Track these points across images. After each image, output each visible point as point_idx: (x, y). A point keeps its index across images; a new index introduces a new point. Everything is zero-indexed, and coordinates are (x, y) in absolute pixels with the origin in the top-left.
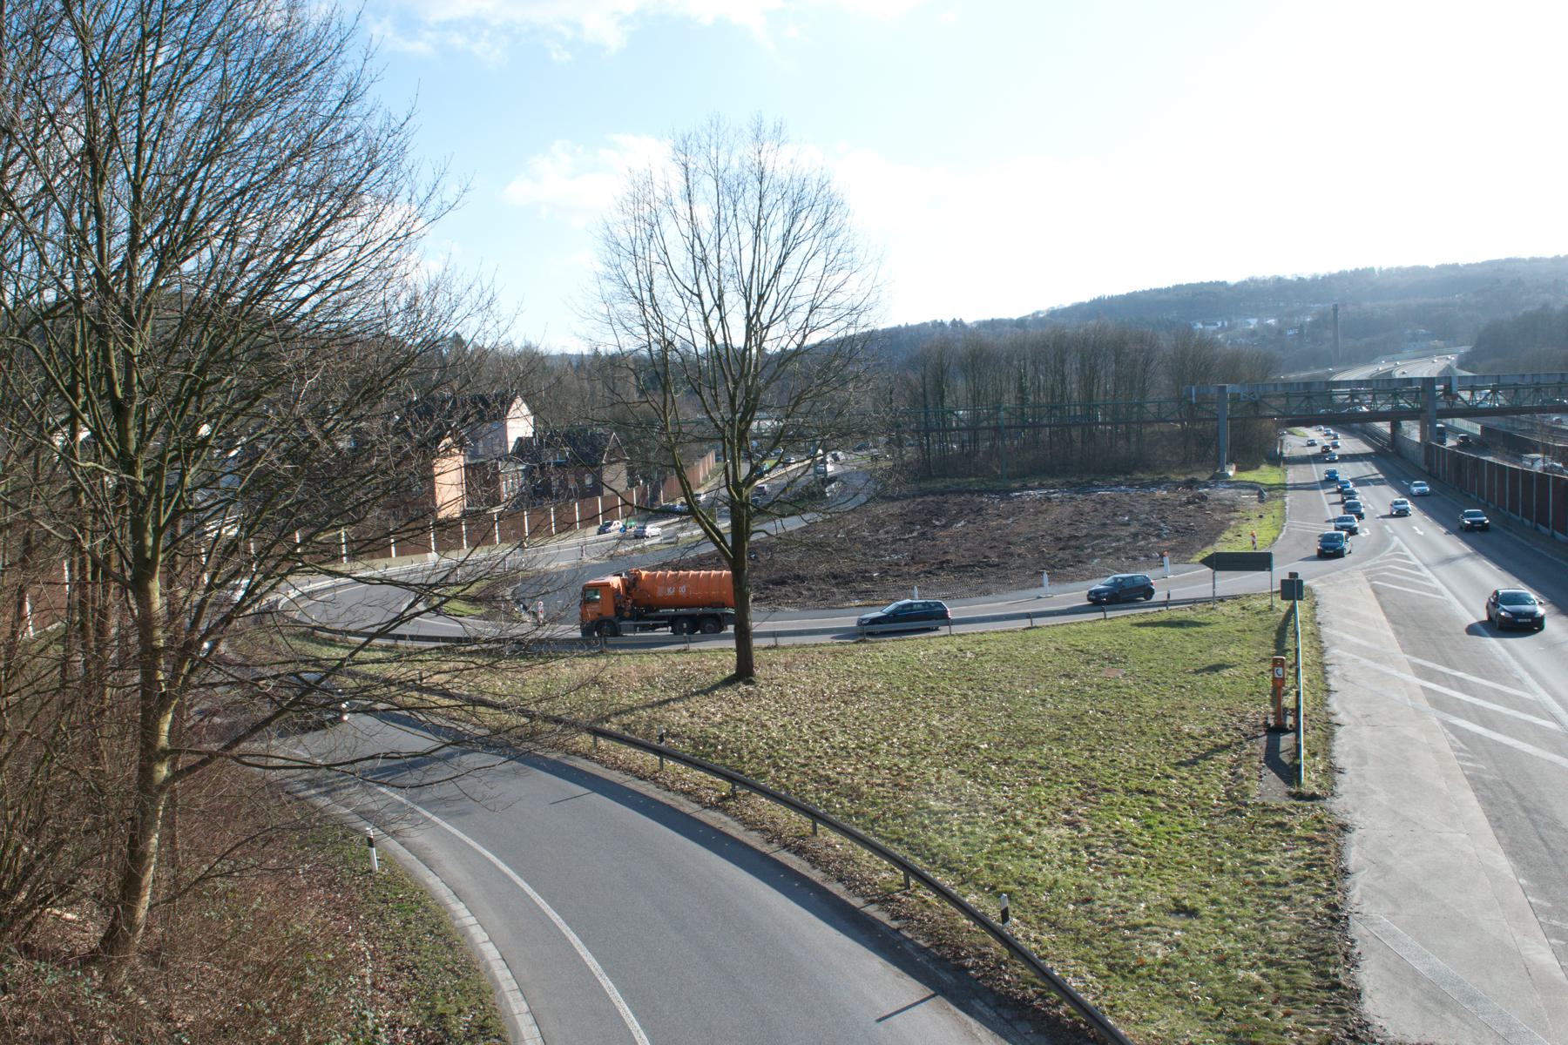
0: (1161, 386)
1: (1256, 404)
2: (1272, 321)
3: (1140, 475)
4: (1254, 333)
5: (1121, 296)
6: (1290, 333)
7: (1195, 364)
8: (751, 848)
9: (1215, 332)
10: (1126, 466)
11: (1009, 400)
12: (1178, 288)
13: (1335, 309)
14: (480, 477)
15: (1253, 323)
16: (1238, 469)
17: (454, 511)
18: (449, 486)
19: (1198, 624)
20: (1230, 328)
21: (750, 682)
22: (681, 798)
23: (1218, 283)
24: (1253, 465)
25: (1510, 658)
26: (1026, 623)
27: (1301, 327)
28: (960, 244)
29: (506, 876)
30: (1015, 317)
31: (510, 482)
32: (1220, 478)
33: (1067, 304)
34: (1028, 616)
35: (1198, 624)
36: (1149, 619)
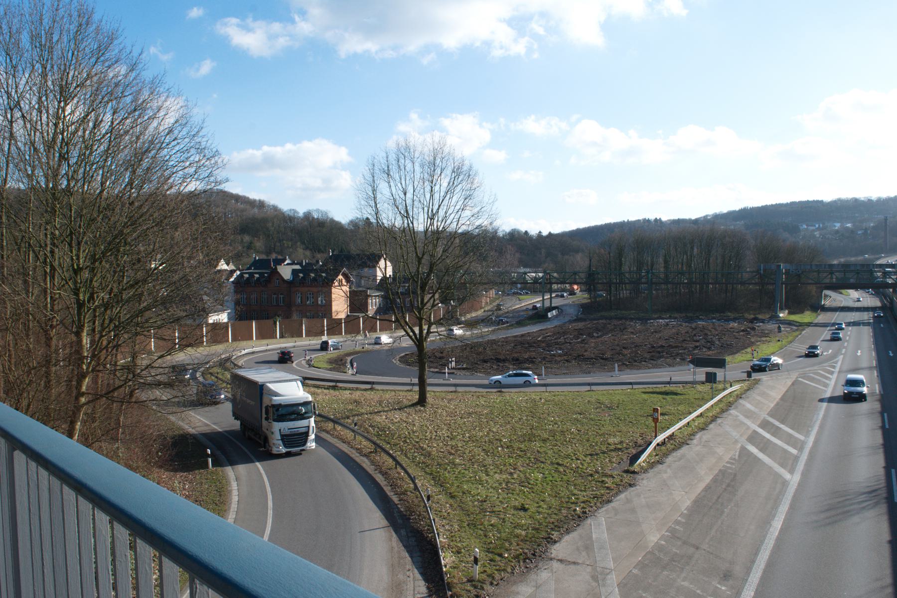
0: (749, 265)
1: (799, 276)
2: (849, 225)
3: (729, 314)
4: (837, 232)
5: (758, 208)
6: (860, 232)
7: (769, 253)
8: (367, 472)
9: (813, 231)
10: (725, 307)
11: (660, 267)
12: (793, 203)
13: (886, 219)
14: (357, 302)
15: (838, 225)
16: (790, 313)
17: (342, 316)
18: (340, 306)
19: (676, 394)
20: (822, 229)
21: (424, 406)
22: (354, 451)
23: (818, 202)
24: (801, 311)
25: (818, 422)
26: (588, 388)
27: (866, 230)
28: (556, 179)
29: (261, 474)
30: (693, 218)
31: (373, 304)
32: (774, 317)
33: (725, 211)
34: (589, 384)
35: (676, 394)
36: (658, 390)
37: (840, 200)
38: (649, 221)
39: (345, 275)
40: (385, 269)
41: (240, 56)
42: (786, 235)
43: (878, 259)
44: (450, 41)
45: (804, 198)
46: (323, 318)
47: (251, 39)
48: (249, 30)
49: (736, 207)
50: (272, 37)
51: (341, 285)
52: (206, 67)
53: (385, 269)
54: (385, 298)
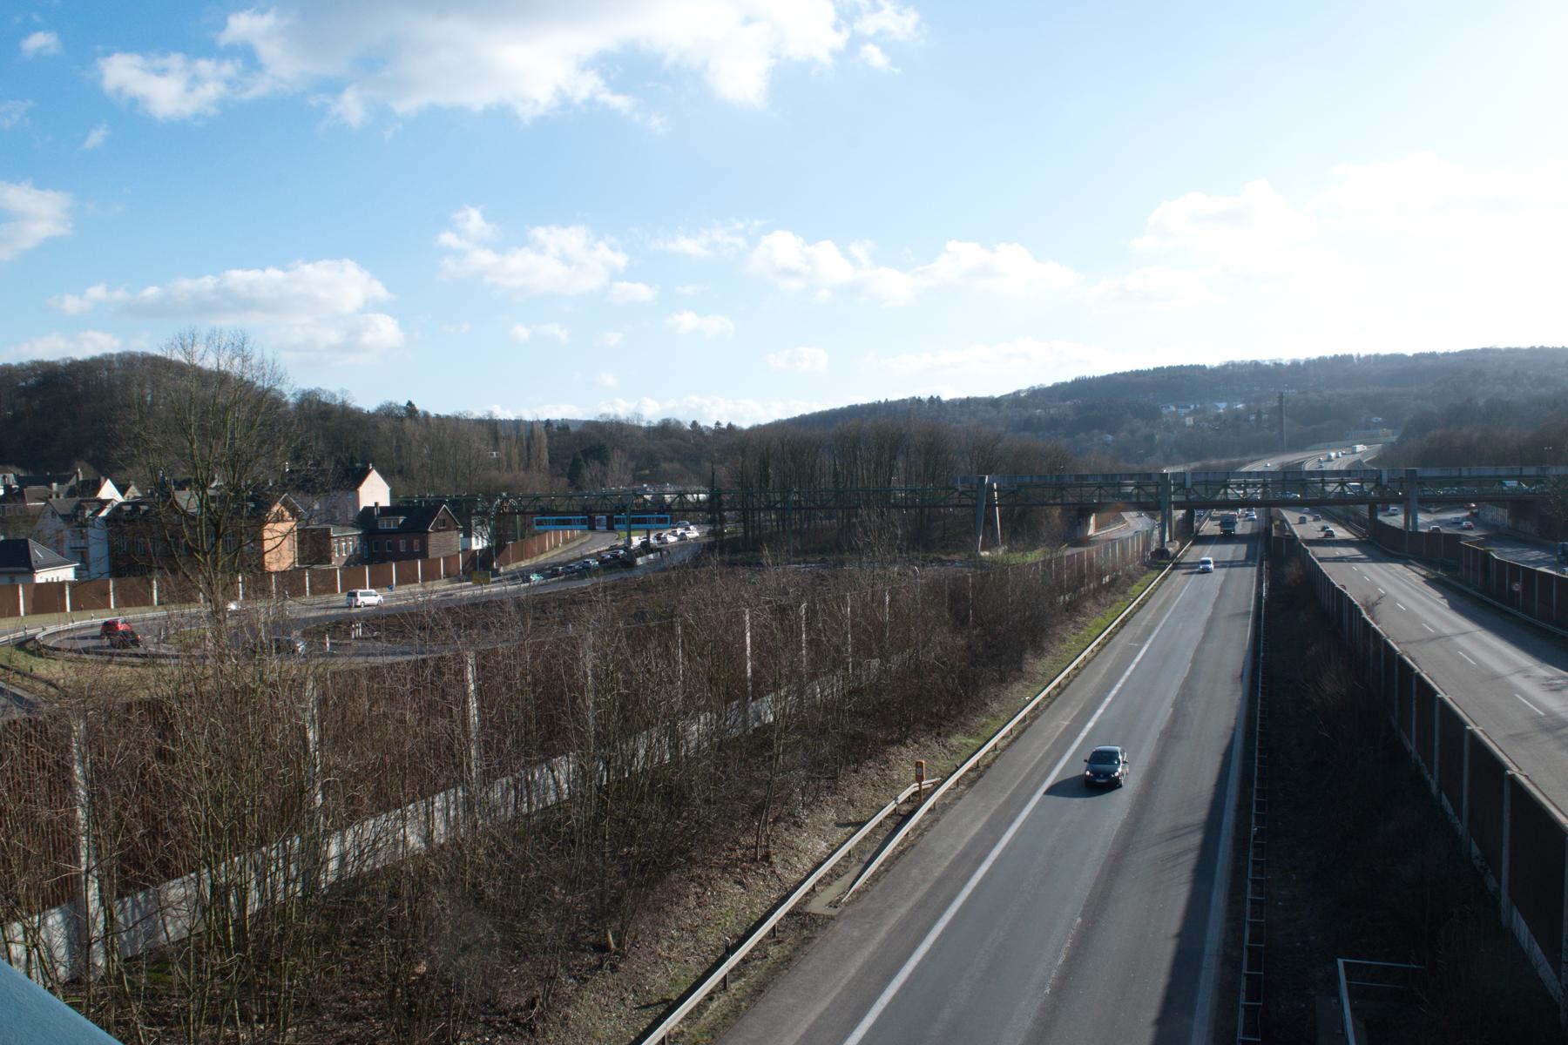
2: (1240, 406)
4: (1218, 417)
12: (1157, 370)
14: (313, 546)
15: (1222, 407)
33: (1049, 384)
37: (1233, 364)
38: (919, 400)
39: (285, 504)
40: (375, 492)
41: (129, 115)
42: (1542, 390)
43: (1243, 464)
44: (478, 98)
45: (1175, 363)
46: (415, 557)
47: (163, 88)
48: (163, 72)
49: (1068, 376)
50: (195, 81)
51: (279, 519)
52: (96, 138)
53: (375, 492)
54: (364, 539)
